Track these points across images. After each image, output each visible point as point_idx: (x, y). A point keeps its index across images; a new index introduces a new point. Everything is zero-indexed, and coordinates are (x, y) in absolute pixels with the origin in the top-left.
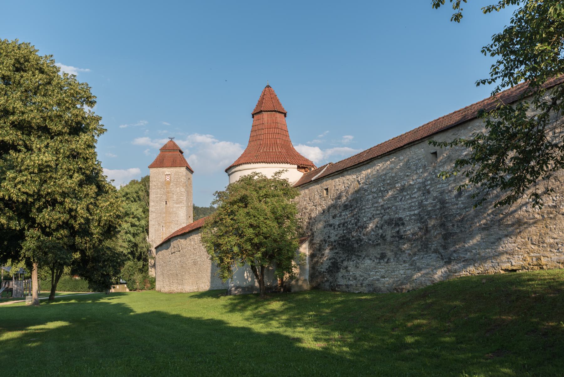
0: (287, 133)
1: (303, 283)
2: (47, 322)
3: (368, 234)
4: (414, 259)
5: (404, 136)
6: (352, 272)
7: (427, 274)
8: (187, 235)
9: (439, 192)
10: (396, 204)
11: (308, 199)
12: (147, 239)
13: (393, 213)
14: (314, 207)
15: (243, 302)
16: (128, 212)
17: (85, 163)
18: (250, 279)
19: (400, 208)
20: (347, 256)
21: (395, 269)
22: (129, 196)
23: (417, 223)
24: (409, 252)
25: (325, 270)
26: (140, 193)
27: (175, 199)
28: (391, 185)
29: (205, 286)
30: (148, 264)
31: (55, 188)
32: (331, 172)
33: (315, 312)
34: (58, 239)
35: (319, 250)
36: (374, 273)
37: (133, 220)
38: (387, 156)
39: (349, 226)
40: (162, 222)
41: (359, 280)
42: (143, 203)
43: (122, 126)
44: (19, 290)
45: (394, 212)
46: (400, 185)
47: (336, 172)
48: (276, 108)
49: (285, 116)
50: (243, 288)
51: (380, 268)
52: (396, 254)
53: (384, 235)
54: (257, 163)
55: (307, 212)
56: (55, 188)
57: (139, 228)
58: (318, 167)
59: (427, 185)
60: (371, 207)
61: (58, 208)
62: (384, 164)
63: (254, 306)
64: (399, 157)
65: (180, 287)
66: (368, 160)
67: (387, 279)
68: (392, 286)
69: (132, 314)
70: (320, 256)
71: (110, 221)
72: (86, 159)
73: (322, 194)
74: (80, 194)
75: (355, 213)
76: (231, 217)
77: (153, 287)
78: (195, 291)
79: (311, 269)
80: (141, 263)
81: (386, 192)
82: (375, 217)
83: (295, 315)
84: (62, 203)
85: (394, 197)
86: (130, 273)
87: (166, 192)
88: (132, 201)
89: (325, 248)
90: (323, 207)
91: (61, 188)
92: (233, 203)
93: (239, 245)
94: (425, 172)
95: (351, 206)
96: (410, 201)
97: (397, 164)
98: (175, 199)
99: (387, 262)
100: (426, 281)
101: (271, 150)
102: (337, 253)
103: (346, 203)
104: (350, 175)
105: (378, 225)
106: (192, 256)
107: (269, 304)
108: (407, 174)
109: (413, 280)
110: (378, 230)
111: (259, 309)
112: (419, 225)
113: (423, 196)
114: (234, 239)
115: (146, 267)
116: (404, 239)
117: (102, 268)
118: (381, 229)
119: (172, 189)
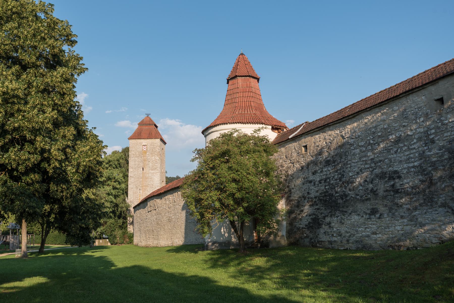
0: (260, 96)
1: (280, 239)
2: (24, 278)
3: (355, 189)
4: (414, 214)
5: (395, 88)
6: (336, 228)
7: (432, 230)
8: (163, 195)
9: (447, 141)
10: (390, 156)
11: (284, 157)
12: (127, 200)
13: (385, 167)
14: (291, 164)
15: (224, 258)
16: (110, 177)
17: (63, 100)
18: (226, 235)
19: (395, 160)
20: (330, 212)
21: (390, 225)
22: (111, 163)
23: (418, 175)
24: (408, 206)
25: (304, 227)
26: (121, 161)
27: (151, 166)
28: (383, 137)
29: (179, 241)
30: (127, 222)
31: (24, 123)
32: (309, 129)
33: (310, 270)
34: (28, 184)
35: (298, 206)
36: (363, 229)
37: (115, 184)
38: (378, 108)
39: (332, 182)
40: (139, 186)
41: (345, 237)
42: (123, 169)
43: (107, 112)
44: (15, 244)
45: (387, 165)
46: (394, 136)
47: (317, 128)
48: (250, 73)
49: (258, 81)
50: (220, 244)
51: (371, 224)
52: (390, 209)
53: (375, 189)
54: (234, 123)
55: (284, 170)
56: (24, 123)
57: (119, 190)
58: (290, 128)
59: (431, 134)
60: (358, 162)
61: (27, 147)
62: (373, 117)
63: (236, 262)
64: (392, 108)
65: (156, 242)
66: (354, 114)
67: (380, 235)
68: (386, 242)
69: (113, 268)
70: (298, 212)
71: (89, 167)
72: (63, 95)
73: (300, 151)
74: (56, 136)
75: (339, 168)
76: (213, 172)
77: (131, 242)
78: (170, 245)
79: (288, 225)
80: (121, 221)
81: (376, 145)
82: (363, 171)
83: (286, 273)
84: (32, 142)
85: (387, 150)
86: (111, 229)
87: (143, 160)
88: (114, 168)
89: (304, 204)
90: (301, 163)
91: (29, 121)
92: (214, 158)
93: (220, 200)
94: (427, 121)
95: (334, 162)
96: (407, 153)
97: (390, 115)
98: (151, 166)
99: (379, 218)
100: (432, 238)
101: (246, 112)
102: (318, 209)
103: (329, 159)
104: (332, 130)
105: (368, 180)
106: (167, 214)
107: (251, 260)
108: (404, 124)
109: (414, 237)
110: (368, 184)
111: (243, 265)
112: (420, 177)
113: (426, 146)
114: (214, 194)
115: (125, 225)
116: (401, 192)
117: (81, 220)
118: (372, 183)
119: (148, 158)
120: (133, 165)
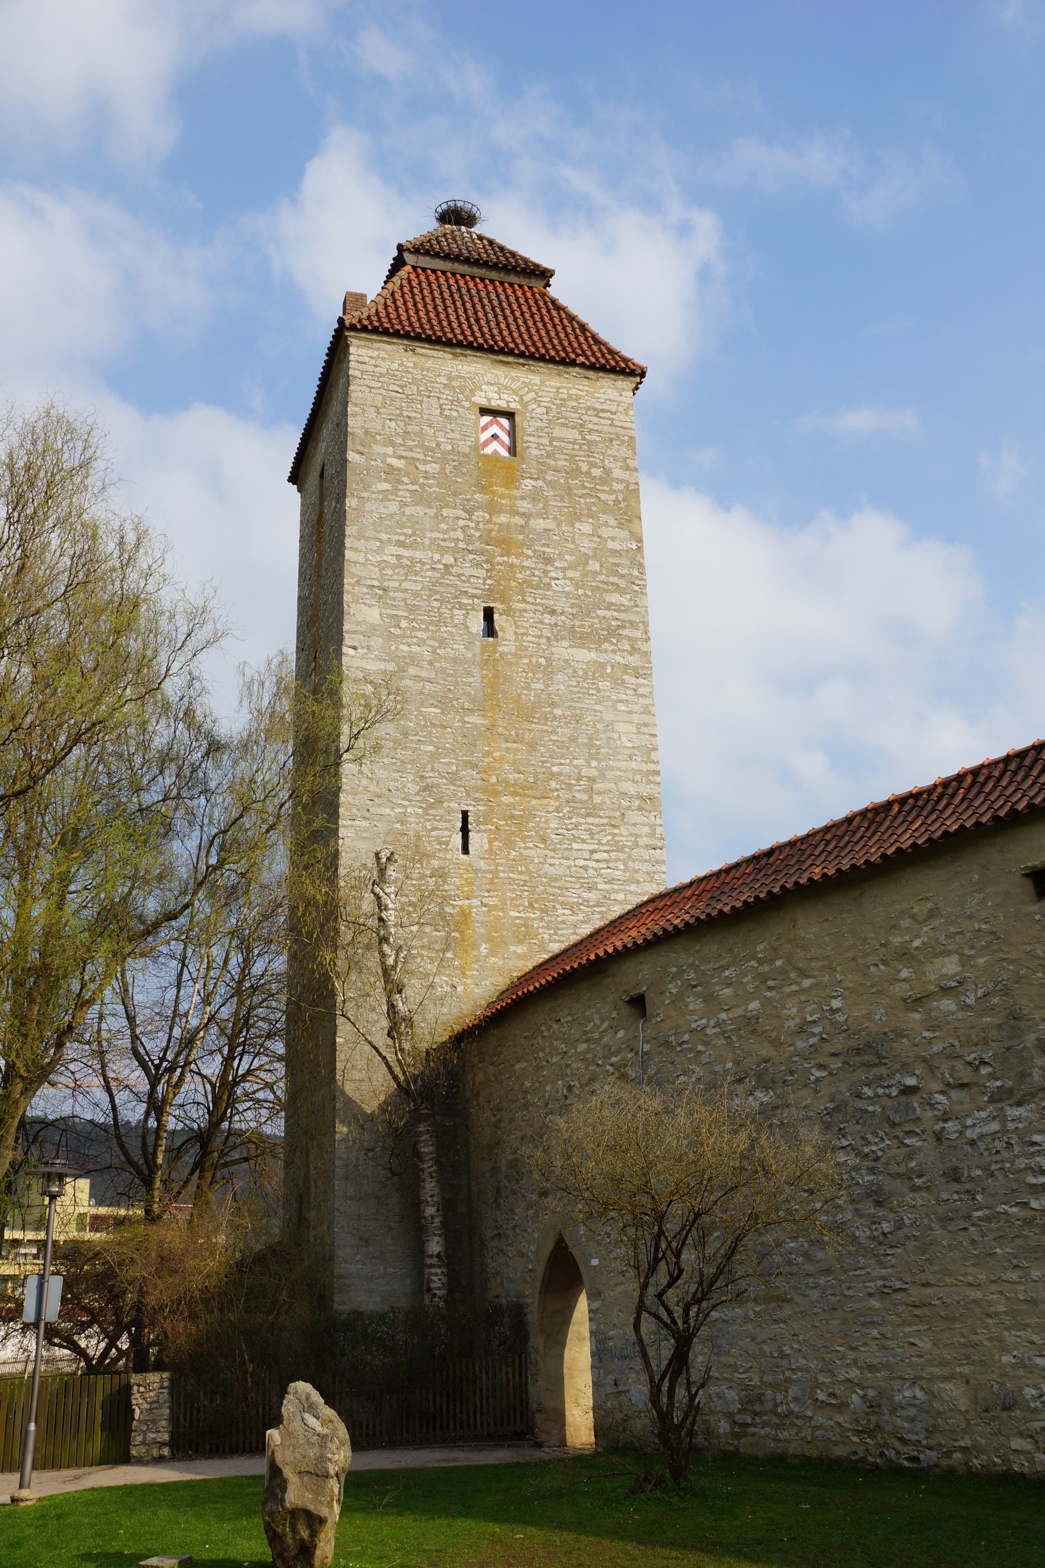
98: (563, 604)
119: (539, 524)
120: (382, 565)
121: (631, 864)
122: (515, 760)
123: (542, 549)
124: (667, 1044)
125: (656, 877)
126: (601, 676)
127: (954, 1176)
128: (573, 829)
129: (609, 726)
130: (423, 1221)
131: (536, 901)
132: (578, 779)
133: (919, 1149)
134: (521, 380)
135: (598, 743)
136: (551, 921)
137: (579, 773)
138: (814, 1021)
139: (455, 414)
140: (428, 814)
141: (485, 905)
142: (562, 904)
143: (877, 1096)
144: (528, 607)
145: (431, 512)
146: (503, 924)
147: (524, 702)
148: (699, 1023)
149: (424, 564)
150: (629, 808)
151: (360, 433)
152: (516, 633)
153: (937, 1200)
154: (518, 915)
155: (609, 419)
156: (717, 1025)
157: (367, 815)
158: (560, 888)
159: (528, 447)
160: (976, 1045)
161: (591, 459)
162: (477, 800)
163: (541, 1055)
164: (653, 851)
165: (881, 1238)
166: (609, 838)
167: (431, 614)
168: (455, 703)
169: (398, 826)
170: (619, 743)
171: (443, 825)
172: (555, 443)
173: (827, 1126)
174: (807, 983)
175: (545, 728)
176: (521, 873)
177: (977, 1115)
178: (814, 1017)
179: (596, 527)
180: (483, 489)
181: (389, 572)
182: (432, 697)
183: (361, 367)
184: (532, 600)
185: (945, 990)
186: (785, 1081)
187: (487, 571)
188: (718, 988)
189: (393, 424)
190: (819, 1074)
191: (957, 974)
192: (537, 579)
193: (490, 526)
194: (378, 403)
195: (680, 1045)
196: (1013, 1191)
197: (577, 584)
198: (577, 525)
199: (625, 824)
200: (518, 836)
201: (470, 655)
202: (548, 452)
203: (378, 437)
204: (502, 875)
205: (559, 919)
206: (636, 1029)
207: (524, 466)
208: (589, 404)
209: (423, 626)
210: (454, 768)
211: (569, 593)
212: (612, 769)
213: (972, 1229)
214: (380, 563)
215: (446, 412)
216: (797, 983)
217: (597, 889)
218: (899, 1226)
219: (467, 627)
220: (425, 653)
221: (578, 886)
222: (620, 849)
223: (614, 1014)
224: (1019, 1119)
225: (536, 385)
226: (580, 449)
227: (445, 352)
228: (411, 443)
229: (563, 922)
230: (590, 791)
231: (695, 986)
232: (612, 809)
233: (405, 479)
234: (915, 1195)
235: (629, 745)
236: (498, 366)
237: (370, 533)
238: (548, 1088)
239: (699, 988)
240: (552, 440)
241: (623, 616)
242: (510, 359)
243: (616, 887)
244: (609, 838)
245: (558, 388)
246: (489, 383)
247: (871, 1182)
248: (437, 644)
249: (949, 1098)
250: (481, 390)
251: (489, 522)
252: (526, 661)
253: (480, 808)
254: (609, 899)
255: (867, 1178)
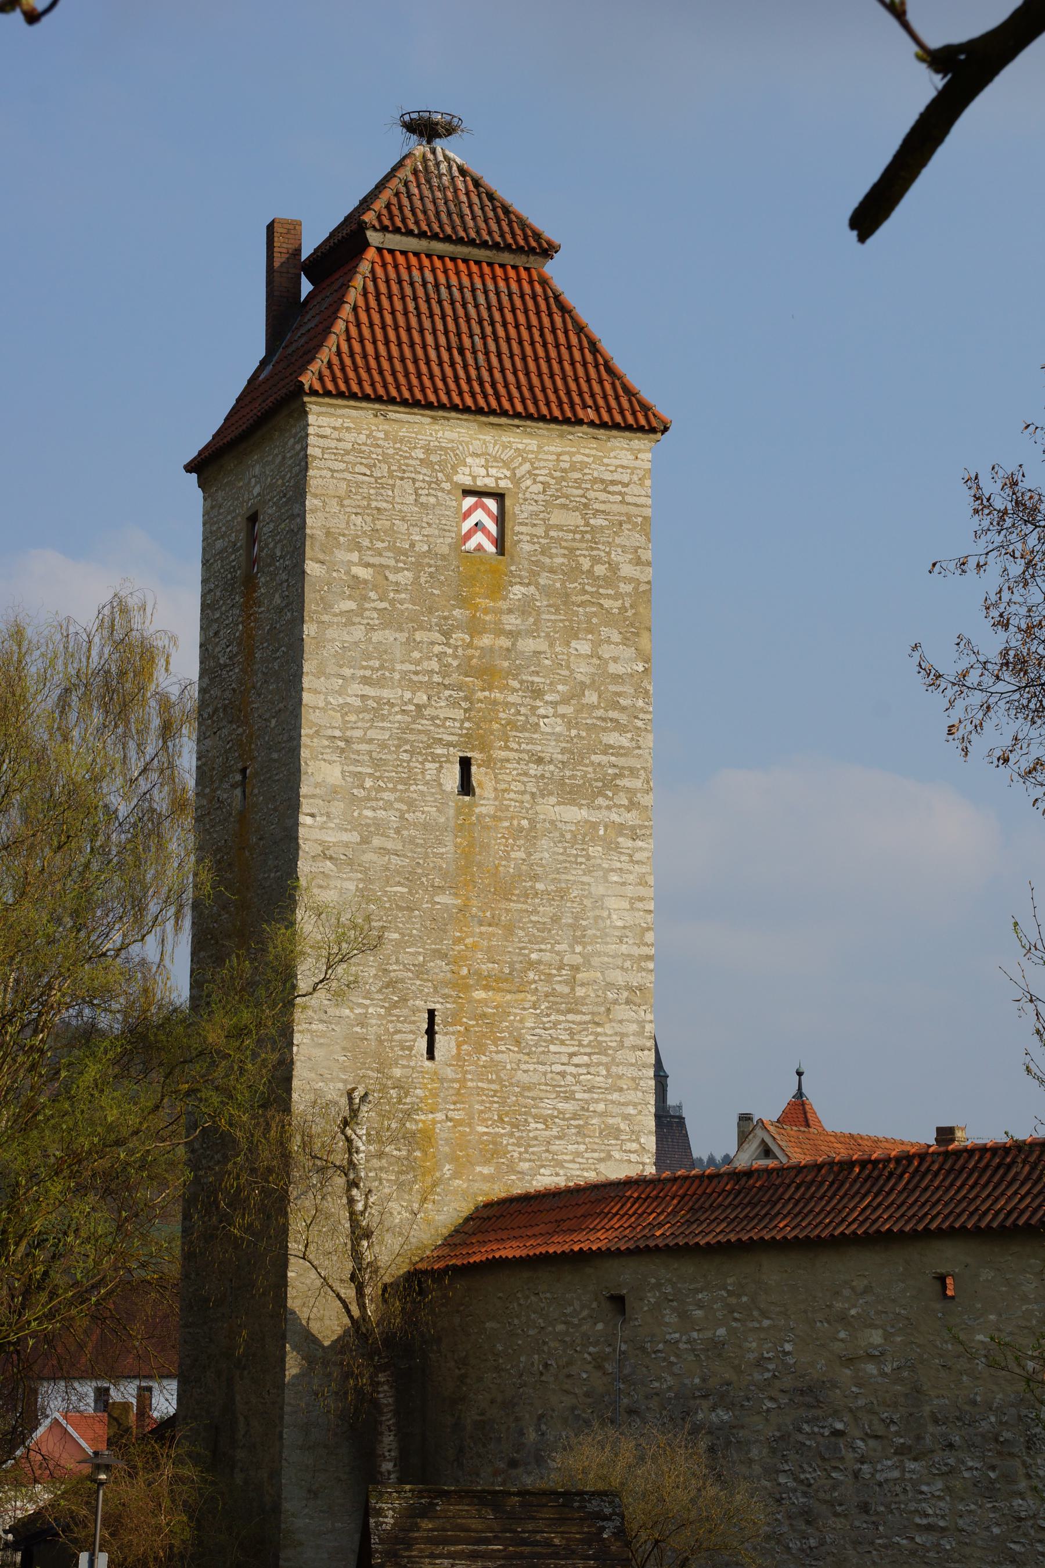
98: (552, 750)
119: (527, 645)
120: (344, 709)
121: (614, 1069)
122: (489, 947)
123: (530, 679)
124: (643, 1349)
125: (642, 1083)
126: (592, 840)
127: (864, 1508)
128: (551, 1028)
129: (599, 902)
130: (379, 1476)
131: (507, 1114)
132: (560, 968)
133: (842, 1482)
134: (514, 446)
135: (584, 923)
136: (522, 1137)
137: (561, 961)
138: (769, 1359)
139: (432, 500)
140: (391, 1015)
141: (451, 1120)
142: (535, 1117)
143: (813, 1433)
144: (511, 755)
145: (402, 637)
146: (469, 1141)
147: (502, 875)
148: (673, 1336)
149: (393, 705)
150: (615, 1002)
151: (319, 534)
152: (496, 789)
153: (851, 1525)
154: (486, 1130)
155: (620, 493)
156: (688, 1342)
157: (324, 1017)
158: (533, 1099)
159: (519, 541)
160: (889, 1406)
161: (595, 553)
162: (445, 996)
163: (516, 1321)
164: (639, 1053)
165: (808, 1551)
166: (591, 1038)
167: (400, 769)
168: (424, 879)
169: (358, 1029)
170: (608, 922)
171: (407, 1027)
172: (552, 533)
173: (773, 1451)
174: (766, 1323)
175: (524, 907)
176: (491, 1082)
177: (885, 1462)
178: (770, 1355)
179: (597, 644)
180: (463, 602)
181: (352, 718)
182: (399, 873)
183: (322, 442)
184: (516, 746)
185: (871, 1357)
186: (742, 1406)
187: (466, 710)
188: (691, 1308)
189: (359, 520)
190: (770, 1405)
191: (880, 1346)
192: (522, 718)
193: (470, 652)
194: (342, 492)
195: (655, 1352)
196: (905, 1527)
197: (569, 722)
198: (574, 644)
199: (611, 1021)
200: (489, 1038)
201: (442, 820)
202: (542, 546)
203: (341, 538)
204: (470, 1084)
205: (531, 1135)
206: (616, 1325)
207: (513, 568)
208: (596, 474)
209: (391, 786)
210: (421, 958)
211: (560, 735)
212: (599, 954)
213: (874, 1552)
214: (342, 706)
215: (423, 499)
216: (760, 1322)
217: (575, 1099)
218: (822, 1543)
219: (440, 785)
220: (392, 817)
221: (554, 1096)
222: (603, 1052)
223: (594, 1305)
224: (913, 1471)
225: (532, 452)
226: (582, 540)
227: (423, 415)
228: (379, 545)
229: (535, 1138)
230: (572, 983)
231: (672, 1301)
232: (597, 1004)
233: (373, 595)
234: (836, 1520)
235: (620, 923)
236: (487, 429)
237: (332, 669)
238: (522, 1359)
239: (675, 1304)
240: (549, 528)
241: (621, 761)
242: (503, 420)
243: (596, 1096)
244: (591, 1038)
245: (559, 455)
246: (475, 455)
247: (804, 1504)
248: (405, 808)
249: (866, 1445)
250: (465, 465)
251: (470, 645)
252: (506, 824)
253: (448, 1006)
254: (588, 1110)
255: (801, 1500)
